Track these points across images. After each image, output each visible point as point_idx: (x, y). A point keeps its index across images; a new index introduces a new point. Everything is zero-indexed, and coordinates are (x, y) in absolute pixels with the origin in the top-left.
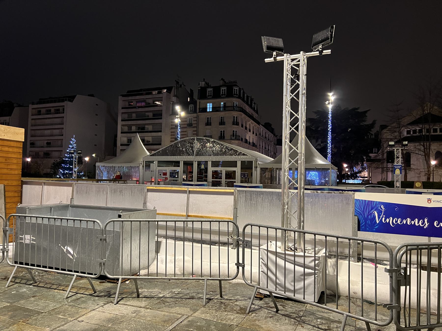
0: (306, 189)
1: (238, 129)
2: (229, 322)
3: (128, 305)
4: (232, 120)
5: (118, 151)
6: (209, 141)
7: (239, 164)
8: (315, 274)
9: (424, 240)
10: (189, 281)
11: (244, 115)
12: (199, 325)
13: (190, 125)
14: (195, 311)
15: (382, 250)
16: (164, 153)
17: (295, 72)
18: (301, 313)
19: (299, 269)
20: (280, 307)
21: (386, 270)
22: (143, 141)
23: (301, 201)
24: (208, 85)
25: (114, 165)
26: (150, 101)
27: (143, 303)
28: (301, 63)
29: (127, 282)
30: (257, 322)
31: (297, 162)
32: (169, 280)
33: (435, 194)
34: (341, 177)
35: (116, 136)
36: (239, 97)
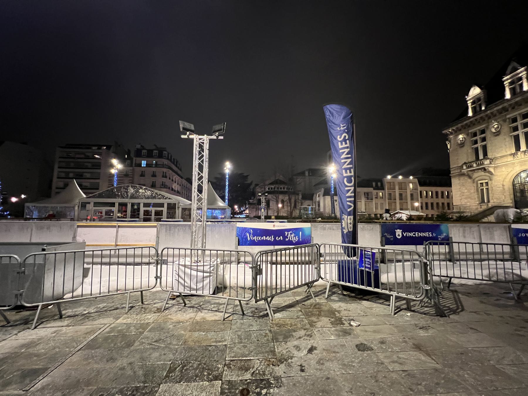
0: (207, 222)
1: (167, 181)
2: (147, 321)
3: (48, 327)
4: (162, 174)
5: (53, 193)
6: (141, 188)
7: (166, 205)
8: (210, 276)
9: (271, 248)
10: (115, 296)
11: (171, 171)
12: (120, 330)
13: (126, 175)
14: (117, 319)
15: (248, 256)
16: (100, 196)
17: (201, 146)
18: (202, 303)
19: (200, 274)
20: (187, 302)
21: (251, 268)
22: (80, 186)
23: (204, 228)
24: (143, 148)
25: (46, 205)
26: (90, 154)
27: (66, 322)
28: (205, 142)
29: (49, 307)
30: (169, 316)
31: (201, 204)
32: (96, 298)
33: (280, 222)
34: (234, 213)
35: (51, 181)
36: (168, 159)
